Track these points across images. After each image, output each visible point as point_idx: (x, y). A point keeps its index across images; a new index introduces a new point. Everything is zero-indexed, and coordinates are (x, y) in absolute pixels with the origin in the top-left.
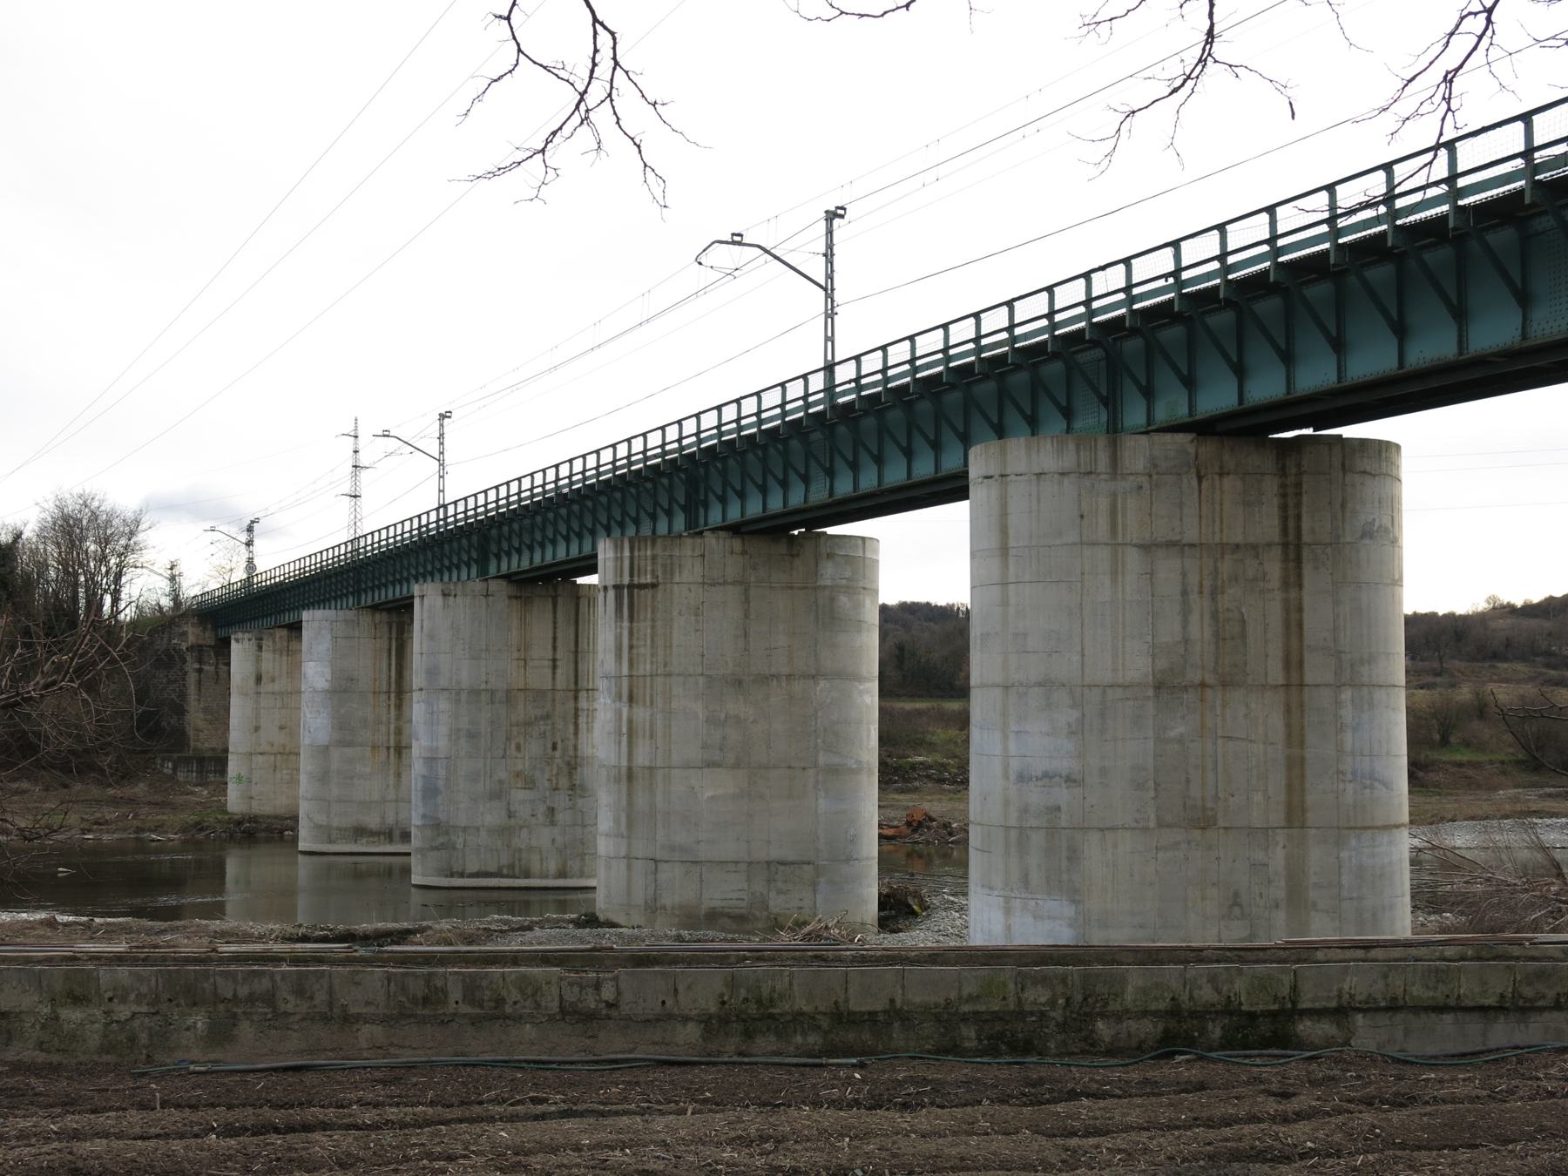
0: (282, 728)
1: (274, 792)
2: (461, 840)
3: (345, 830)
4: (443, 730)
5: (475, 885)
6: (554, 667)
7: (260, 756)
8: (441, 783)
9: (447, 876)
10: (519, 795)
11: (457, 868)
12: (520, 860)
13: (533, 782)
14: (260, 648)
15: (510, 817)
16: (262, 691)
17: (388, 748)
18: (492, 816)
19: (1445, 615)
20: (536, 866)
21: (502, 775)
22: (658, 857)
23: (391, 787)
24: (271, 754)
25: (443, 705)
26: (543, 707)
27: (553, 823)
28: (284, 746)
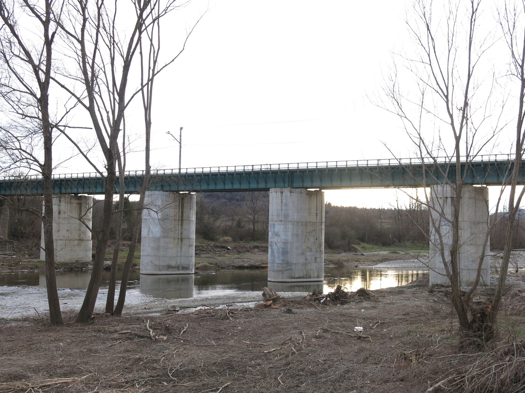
0: (68, 231)
1: (65, 254)
2: (294, 268)
3: (164, 266)
4: (290, 234)
5: (297, 281)
6: (317, 216)
7: (60, 241)
8: (289, 250)
9: (290, 278)
10: (308, 254)
11: (293, 276)
12: (308, 273)
13: (312, 250)
14: (60, 201)
15: (306, 260)
16: (61, 217)
17: (178, 239)
18: (302, 260)
19: (334, 207)
20: (312, 276)
21: (304, 247)
22: (463, 269)
23: (179, 252)
24: (64, 240)
25: (290, 226)
26: (314, 227)
27: (316, 262)
28: (69, 237)
